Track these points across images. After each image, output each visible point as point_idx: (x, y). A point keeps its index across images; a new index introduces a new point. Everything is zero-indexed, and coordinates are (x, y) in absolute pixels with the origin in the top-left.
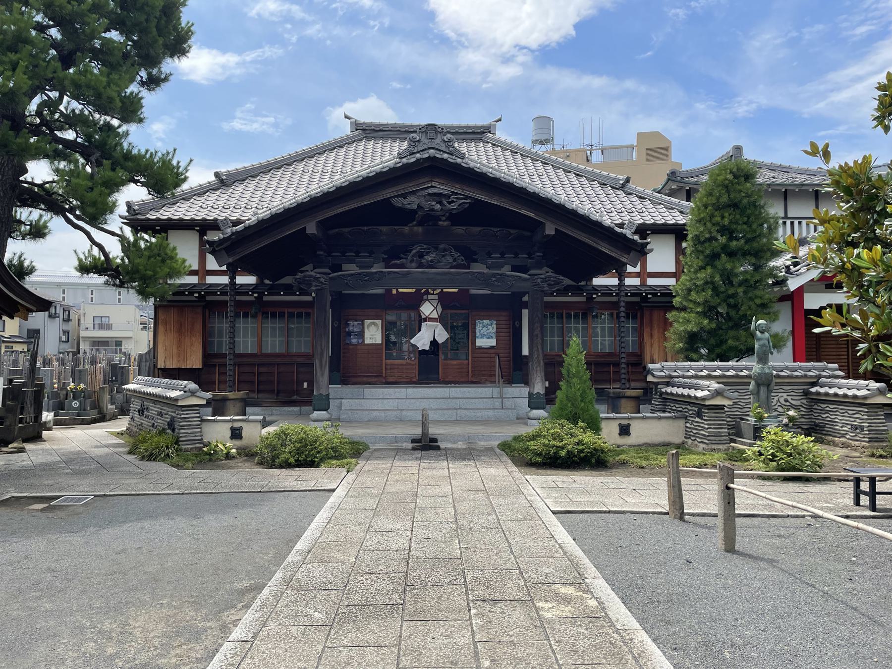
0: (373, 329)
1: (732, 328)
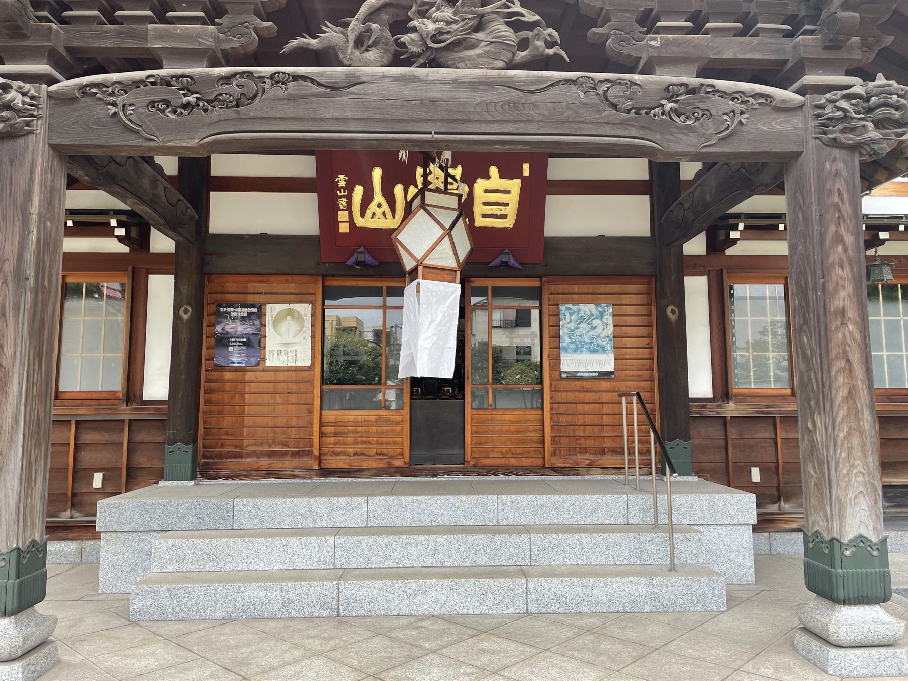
0: (289, 327)
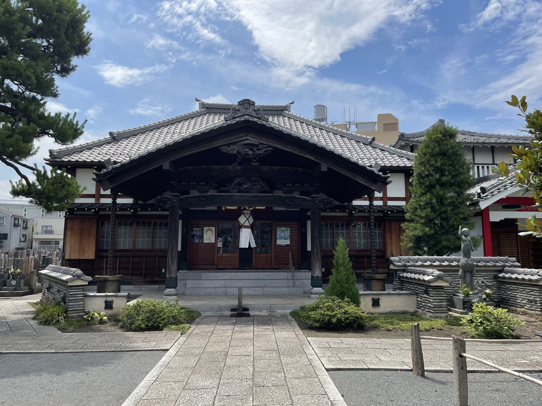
0: (209, 233)
1: (444, 234)
